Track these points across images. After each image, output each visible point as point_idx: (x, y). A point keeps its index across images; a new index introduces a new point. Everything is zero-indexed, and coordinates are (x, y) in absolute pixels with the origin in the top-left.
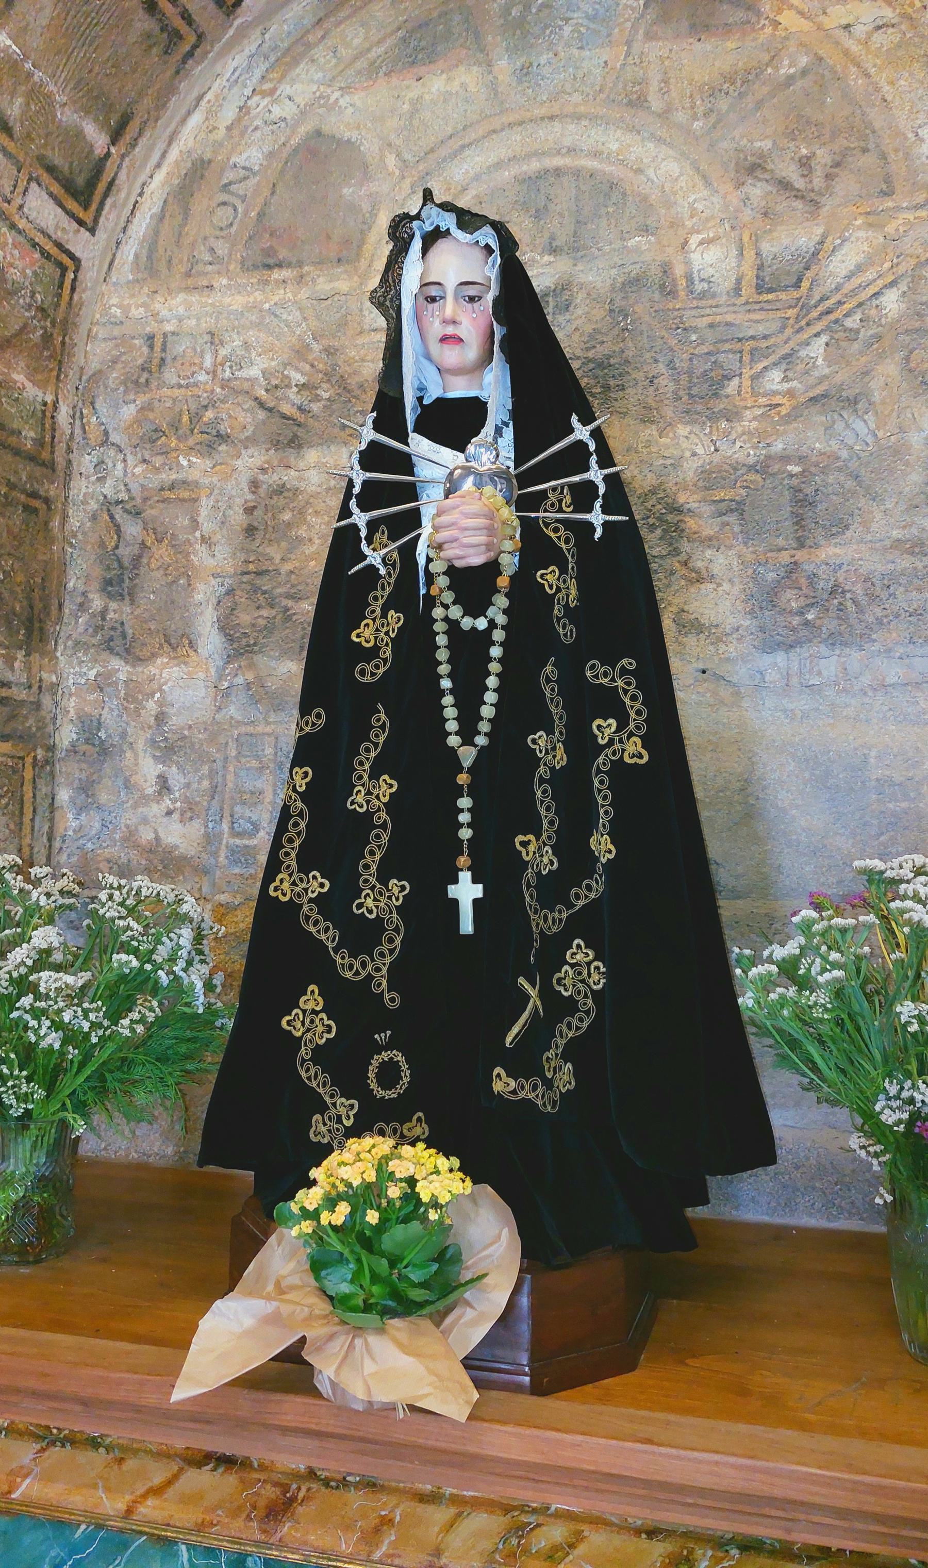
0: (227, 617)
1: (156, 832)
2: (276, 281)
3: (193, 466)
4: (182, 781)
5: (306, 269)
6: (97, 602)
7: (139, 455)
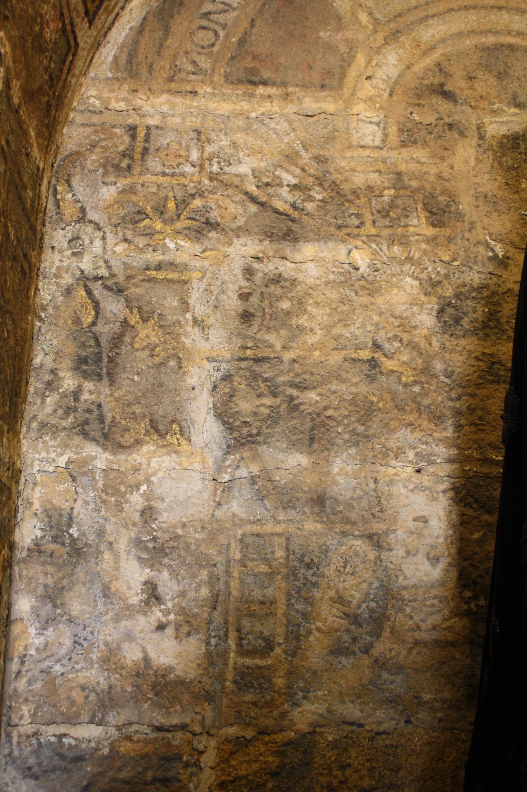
0: (225, 404)
1: (144, 651)
2: (262, 96)
3: (180, 248)
4: (176, 588)
5: (291, 89)
6: (69, 381)
7: (121, 234)
